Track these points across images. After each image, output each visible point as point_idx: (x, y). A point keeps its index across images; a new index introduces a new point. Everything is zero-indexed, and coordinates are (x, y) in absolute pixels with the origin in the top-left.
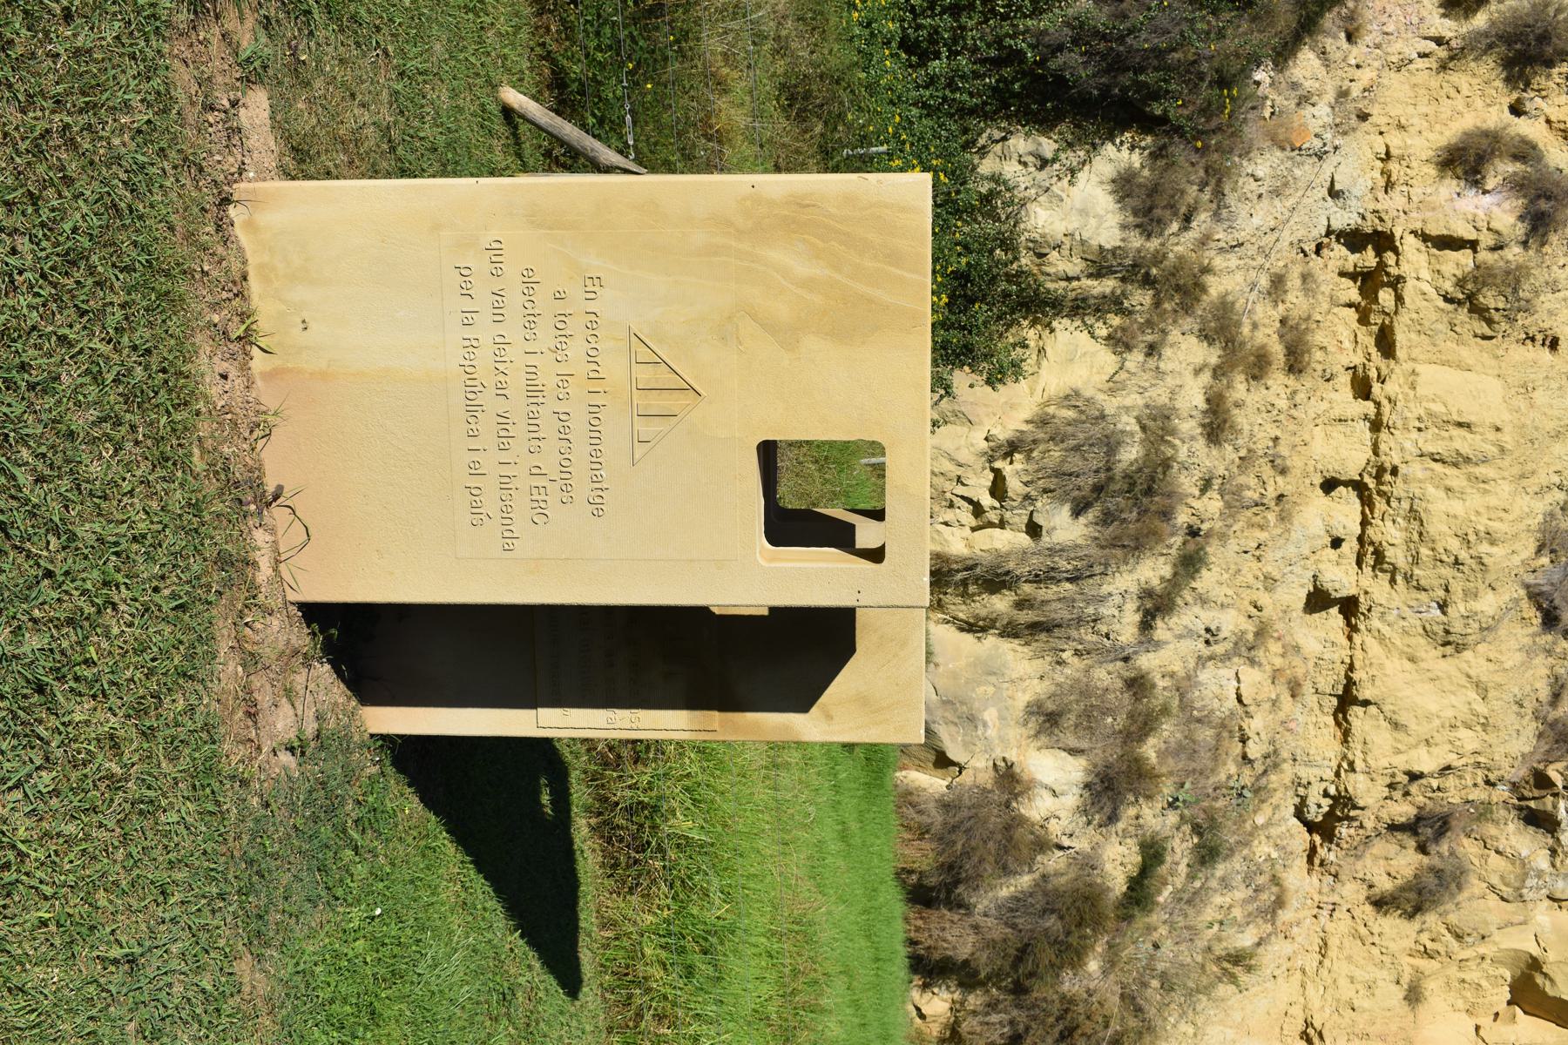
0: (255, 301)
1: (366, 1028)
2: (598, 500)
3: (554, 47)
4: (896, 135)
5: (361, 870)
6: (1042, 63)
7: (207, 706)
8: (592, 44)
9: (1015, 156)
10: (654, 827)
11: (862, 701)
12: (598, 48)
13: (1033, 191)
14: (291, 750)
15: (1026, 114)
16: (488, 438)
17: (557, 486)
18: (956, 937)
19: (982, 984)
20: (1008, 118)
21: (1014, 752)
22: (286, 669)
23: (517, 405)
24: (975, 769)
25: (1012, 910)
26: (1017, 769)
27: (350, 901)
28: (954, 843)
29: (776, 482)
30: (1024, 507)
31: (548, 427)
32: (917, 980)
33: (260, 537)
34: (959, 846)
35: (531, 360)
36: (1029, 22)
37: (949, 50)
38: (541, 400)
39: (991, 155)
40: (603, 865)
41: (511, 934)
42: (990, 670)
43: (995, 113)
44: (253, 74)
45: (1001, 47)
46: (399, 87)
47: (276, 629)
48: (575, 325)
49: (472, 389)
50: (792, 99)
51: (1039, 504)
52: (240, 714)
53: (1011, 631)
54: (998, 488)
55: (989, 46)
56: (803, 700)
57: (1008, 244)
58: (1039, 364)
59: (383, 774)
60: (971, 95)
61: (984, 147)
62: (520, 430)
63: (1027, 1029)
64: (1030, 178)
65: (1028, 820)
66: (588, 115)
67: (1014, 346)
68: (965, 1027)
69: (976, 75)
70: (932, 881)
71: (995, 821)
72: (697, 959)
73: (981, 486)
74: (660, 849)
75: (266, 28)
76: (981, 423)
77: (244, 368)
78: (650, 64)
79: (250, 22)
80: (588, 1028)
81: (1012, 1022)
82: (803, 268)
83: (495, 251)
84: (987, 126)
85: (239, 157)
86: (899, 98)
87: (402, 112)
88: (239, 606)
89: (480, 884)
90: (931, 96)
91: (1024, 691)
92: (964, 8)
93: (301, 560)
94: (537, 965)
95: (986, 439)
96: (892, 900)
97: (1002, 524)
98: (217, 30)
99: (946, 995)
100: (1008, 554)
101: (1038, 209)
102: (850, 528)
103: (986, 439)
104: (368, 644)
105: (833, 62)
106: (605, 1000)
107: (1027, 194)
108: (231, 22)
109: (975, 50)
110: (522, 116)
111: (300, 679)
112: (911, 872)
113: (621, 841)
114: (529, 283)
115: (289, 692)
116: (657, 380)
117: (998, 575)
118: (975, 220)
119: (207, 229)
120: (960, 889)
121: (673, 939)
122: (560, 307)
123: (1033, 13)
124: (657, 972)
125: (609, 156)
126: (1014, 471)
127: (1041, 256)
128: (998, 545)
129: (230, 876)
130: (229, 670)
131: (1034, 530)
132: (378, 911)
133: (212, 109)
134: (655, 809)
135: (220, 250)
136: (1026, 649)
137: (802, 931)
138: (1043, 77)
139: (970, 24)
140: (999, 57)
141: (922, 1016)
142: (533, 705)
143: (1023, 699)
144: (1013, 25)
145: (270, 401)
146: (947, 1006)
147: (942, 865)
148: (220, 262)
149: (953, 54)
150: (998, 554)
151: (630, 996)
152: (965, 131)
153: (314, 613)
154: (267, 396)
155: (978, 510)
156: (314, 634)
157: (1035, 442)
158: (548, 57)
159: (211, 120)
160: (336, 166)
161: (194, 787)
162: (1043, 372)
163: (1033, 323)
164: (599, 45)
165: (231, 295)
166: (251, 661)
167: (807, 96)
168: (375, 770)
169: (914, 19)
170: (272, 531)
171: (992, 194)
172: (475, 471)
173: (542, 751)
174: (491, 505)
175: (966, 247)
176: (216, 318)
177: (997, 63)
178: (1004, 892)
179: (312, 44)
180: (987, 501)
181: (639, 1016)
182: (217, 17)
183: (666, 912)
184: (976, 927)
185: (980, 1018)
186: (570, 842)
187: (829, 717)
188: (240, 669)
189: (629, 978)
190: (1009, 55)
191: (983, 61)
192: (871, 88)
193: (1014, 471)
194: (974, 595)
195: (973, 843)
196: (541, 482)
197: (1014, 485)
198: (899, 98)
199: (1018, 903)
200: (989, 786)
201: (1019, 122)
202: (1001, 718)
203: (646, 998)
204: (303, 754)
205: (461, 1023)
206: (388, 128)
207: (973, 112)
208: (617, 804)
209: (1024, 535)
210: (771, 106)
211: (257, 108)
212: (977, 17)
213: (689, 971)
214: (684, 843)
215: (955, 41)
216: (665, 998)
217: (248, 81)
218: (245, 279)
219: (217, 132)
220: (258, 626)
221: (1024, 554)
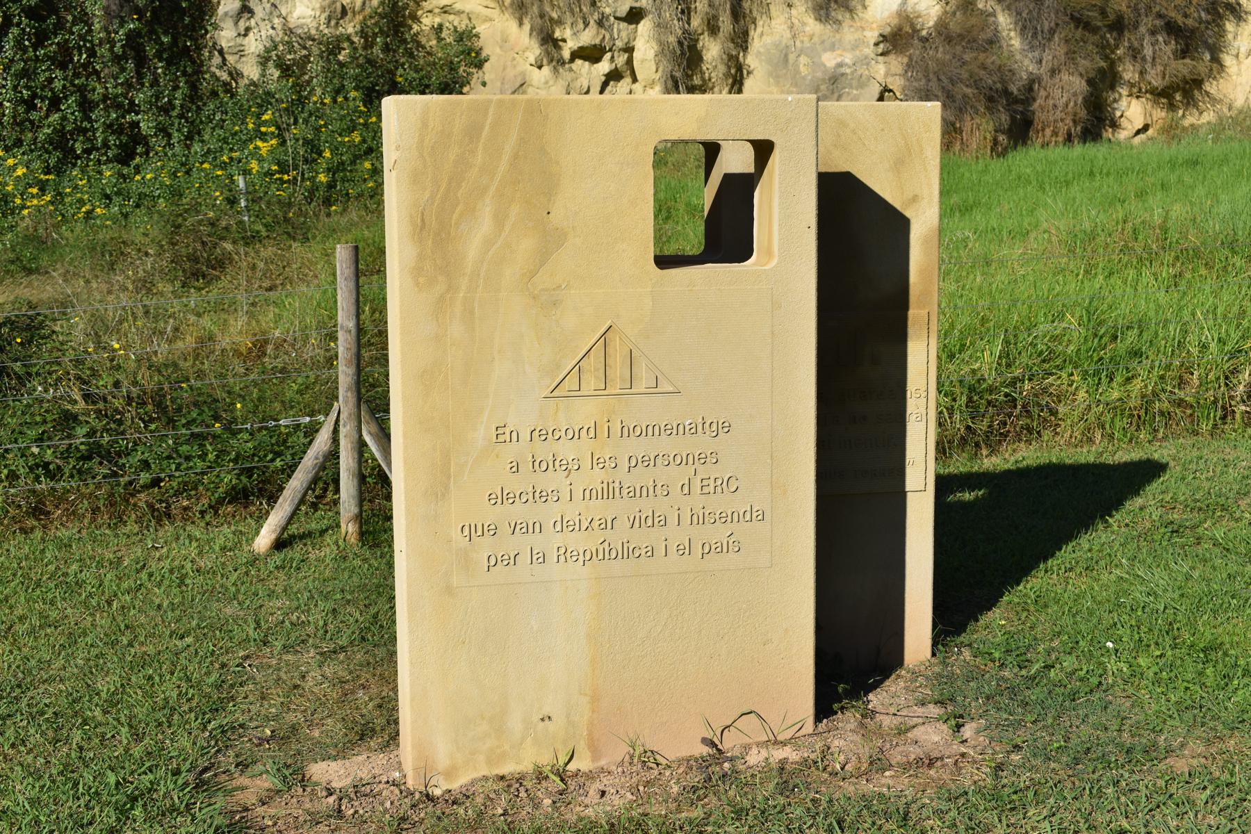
0: (526, 766)
1: (1226, 654)
2: (714, 427)
3: (205, 501)
4: (223, 166)
5: (1069, 663)
6: (140, 12)
7: (932, 800)
8: (200, 464)
9: (239, 40)
10: (991, 390)
11: (899, 164)
12: (203, 457)
13: (276, 21)
14: (959, 726)
15: (194, 30)
16: (654, 537)
17: (701, 468)
18: (1064, 92)
19: (1112, 64)
20: (199, 49)
21: (868, 34)
22: (879, 732)
23: (621, 508)
24: (886, 75)
25: (1035, 35)
26: (887, 30)
27: (1101, 671)
28: (965, 96)
29: (683, 256)
30: (611, 26)
31: (643, 477)
32: (1108, 133)
33: (755, 758)
34: (969, 91)
35: (578, 495)
36: (97, 26)
37: (129, 112)
38: (617, 485)
39: (239, 66)
40: (1029, 442)
41: (1110, 526)
42: (782, 61)
43: (194, 62)
44: (294, 777)
45: (124, 57)
46: (278, 645)
47: (842, 742)
48: (543, 451)
49: (606, 553)
50: (196, 275)
51: (608, 10)
52: (932, 772)
53: (741, 40)
54: (591, 54)
55: (123, 70)
56: (900, 224)
57: (332, 47)
58: (459, 13)
59: (970, 645)
60: (176, 88)
61: (230, 74)
62: (646, 506)
63: (1159, 16)
64: (262, 24)
65: (940, 19)
66: (272, 466)
67: (440, 39)
68: (1157, 82)
69: (155, 83)
70: (1005, 118)
71: (942, 53)
72: (1121, 347)
73: (589, 72)
74: (1013, 383)
75: (247, 766)
76: (523, 74)
77: (590, 776)
78: (211, 406)
79: (243, 781)
80: (1195, 453)
81: (1153, 33)
82: (484, 225)
83: (471, 532)
84: (208, 71)
85: (381, 786)
86: (183, 164)
87: (303, 642)
88: (826, 775)
89: (1066, 554)
90: (179, 130)
91: (804, 24)
92: (83, 97)
93: (774, 720)
94: (1139, 501)
95: (540, 67)
96: (1027, 159)
97: (629, 50)
98: (260, 810)
99: (1123, 103)
100: (660, 43)
101: (295, 15)
102: (728, 179)
103: (540, 67)
104: (851, 659)
105: (155, 232)
106: (1165, 438)
107: (279, 27)
108: (250, 798)
109: (128, 85)
110: (284, 529)
111: (887, 721)
112: (995, 142)
113: (1005, 424)
114: (503, 498)
115: (902, 731)
116: (597, 370)
117: (683, 54)
118: (309, 82)
119: (462, 811)
120: (1014, 89)
121: (1101, 373)
122: (526, 467)
123: (86, 23)
124: (1137, 384)
125: (322, 441)
126: (573, 38)
127: (344, 11)
128: (651, 54)
129: (1096, 776)
130: (886, 782)
131: (634, 16)
132: (1110, 644)
133: (340, 811)
134: (972, 389)
135: (479, 800)
136: (760, 23)
137: (1082, 243)
138: (154, 12)
139: (100, 90)
140: (134, 58)
141: (1145, 128)
142: (902, 495)
143: (812, 25)
144: (100, 44)
145: (622, 751)
146: (1134, 101)
147: (987, 108)
148: (492, 800)
149: (133, 108)
150: (661, 53)
151: (1162, 413)
152: (214, 94)
153: (824, 709)
154: (615, 753)
155: (614, 76)
156: (842, 708)
157: (542, 16)
158: (215, 508)
159: (352, 811)
160: (371, 699)
161: (1012, 809)
162: (468, 7)
163: (416, 19)
164: (199, 457)
165: (522, 789)
166: (878, 764)
167: (194, 259)
168: (967, 653)
169: (97, 149)
170: (747, 748)
171: (280, 65)
172: (685, 550)
173: (944, 485)
174: (719, 533)
175: (338, 92)
176: (547, 802)
177: (141, 61)
178: (1016, 43)
179: (252, 725)
180: (604, 66)
181: (1180, 403)
182: (246, 809)
183: (1076, 378)
184: (1053, 72)
185: (1148, 66)
186: (1009, 472)
187: (915, 199)
188: (887, 773)
189: (1142, 413)
190: (132, 48)
191: (140, 76)
192: (176, 193)
193: (573, 38)
194: (703, 79)
195: (965, 75)
196: (697, 484)
197: (588, 37)
198: (183, 164)
199: (1027, 27)
200: (905, 60)
201: (203, 36)
202: (832, 48)
203: (1163, 396)
204: (961, 716)
205: (1208, 570)
206: (322, 654)
207: (193, 86)
208: (968, 428)
209: (641, 26)
210: (214, 293)
211: (330, 772)
212: (93, 83)
213: (1136, 354)
214: (1007, 360)
215: (119, 106)
216: (1162, 377)
217: (304, 781)
218: (502, 778)
219: (362, 807)
220: (842, 758)
221: (660, 26)
